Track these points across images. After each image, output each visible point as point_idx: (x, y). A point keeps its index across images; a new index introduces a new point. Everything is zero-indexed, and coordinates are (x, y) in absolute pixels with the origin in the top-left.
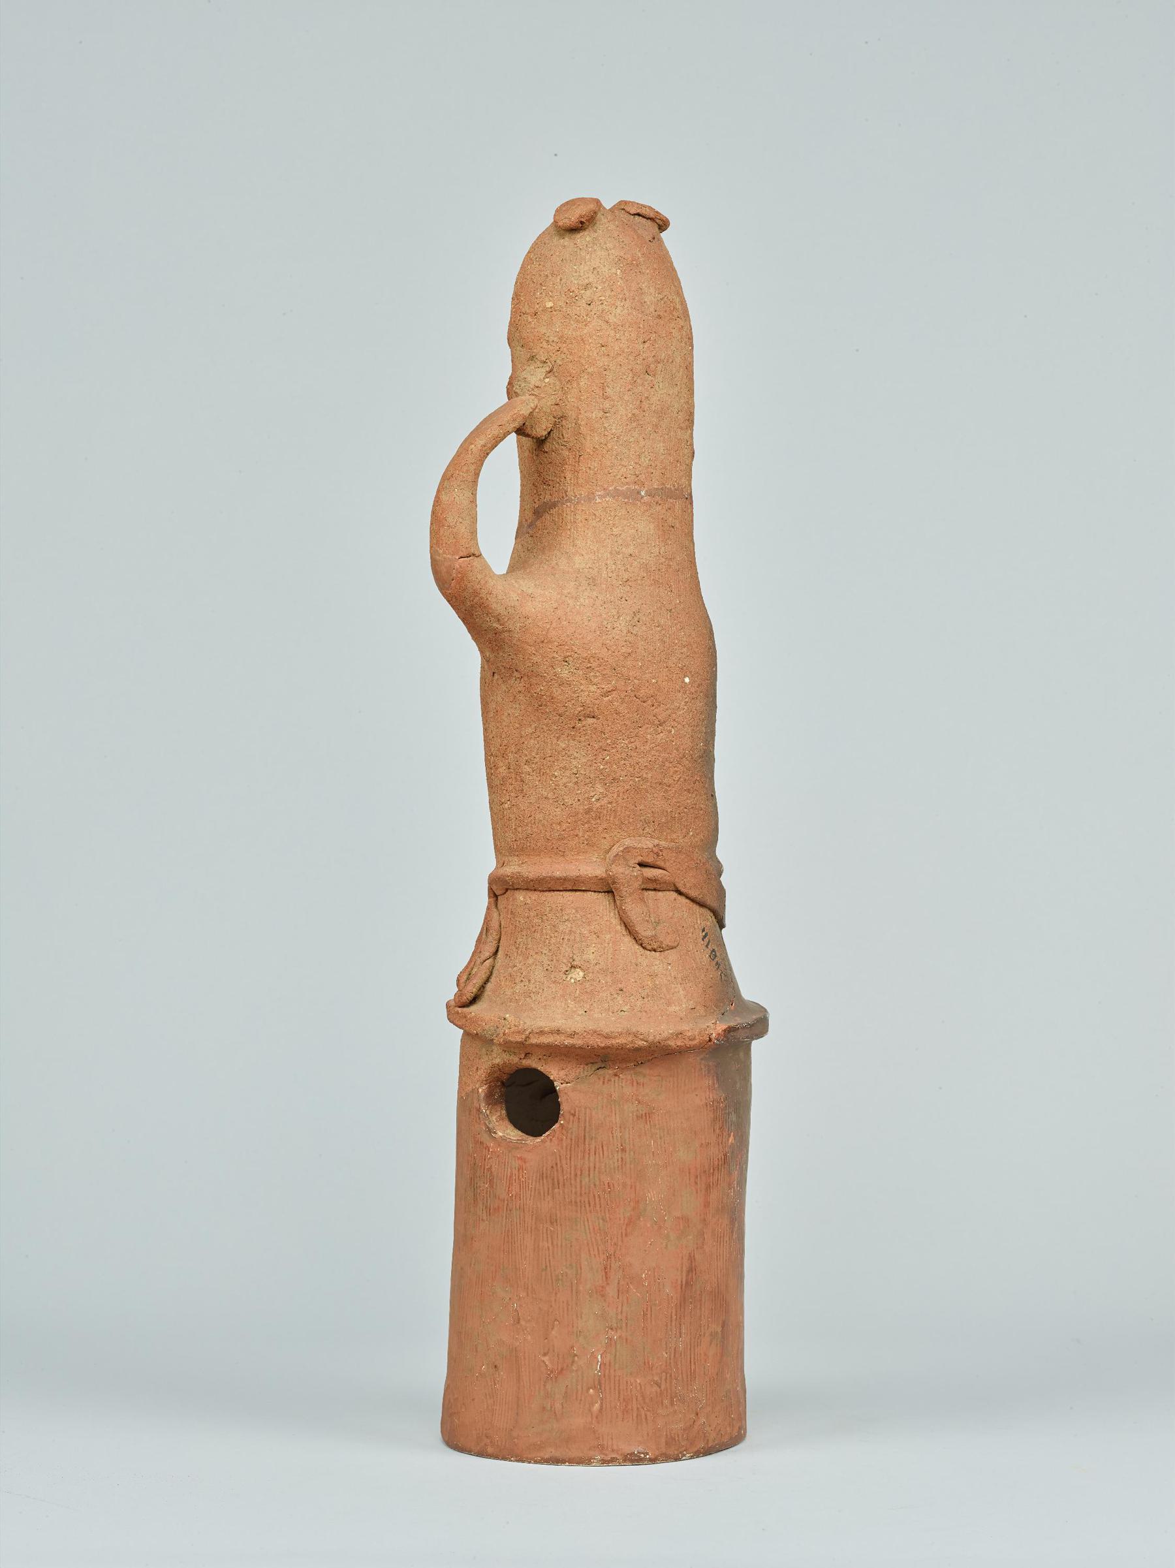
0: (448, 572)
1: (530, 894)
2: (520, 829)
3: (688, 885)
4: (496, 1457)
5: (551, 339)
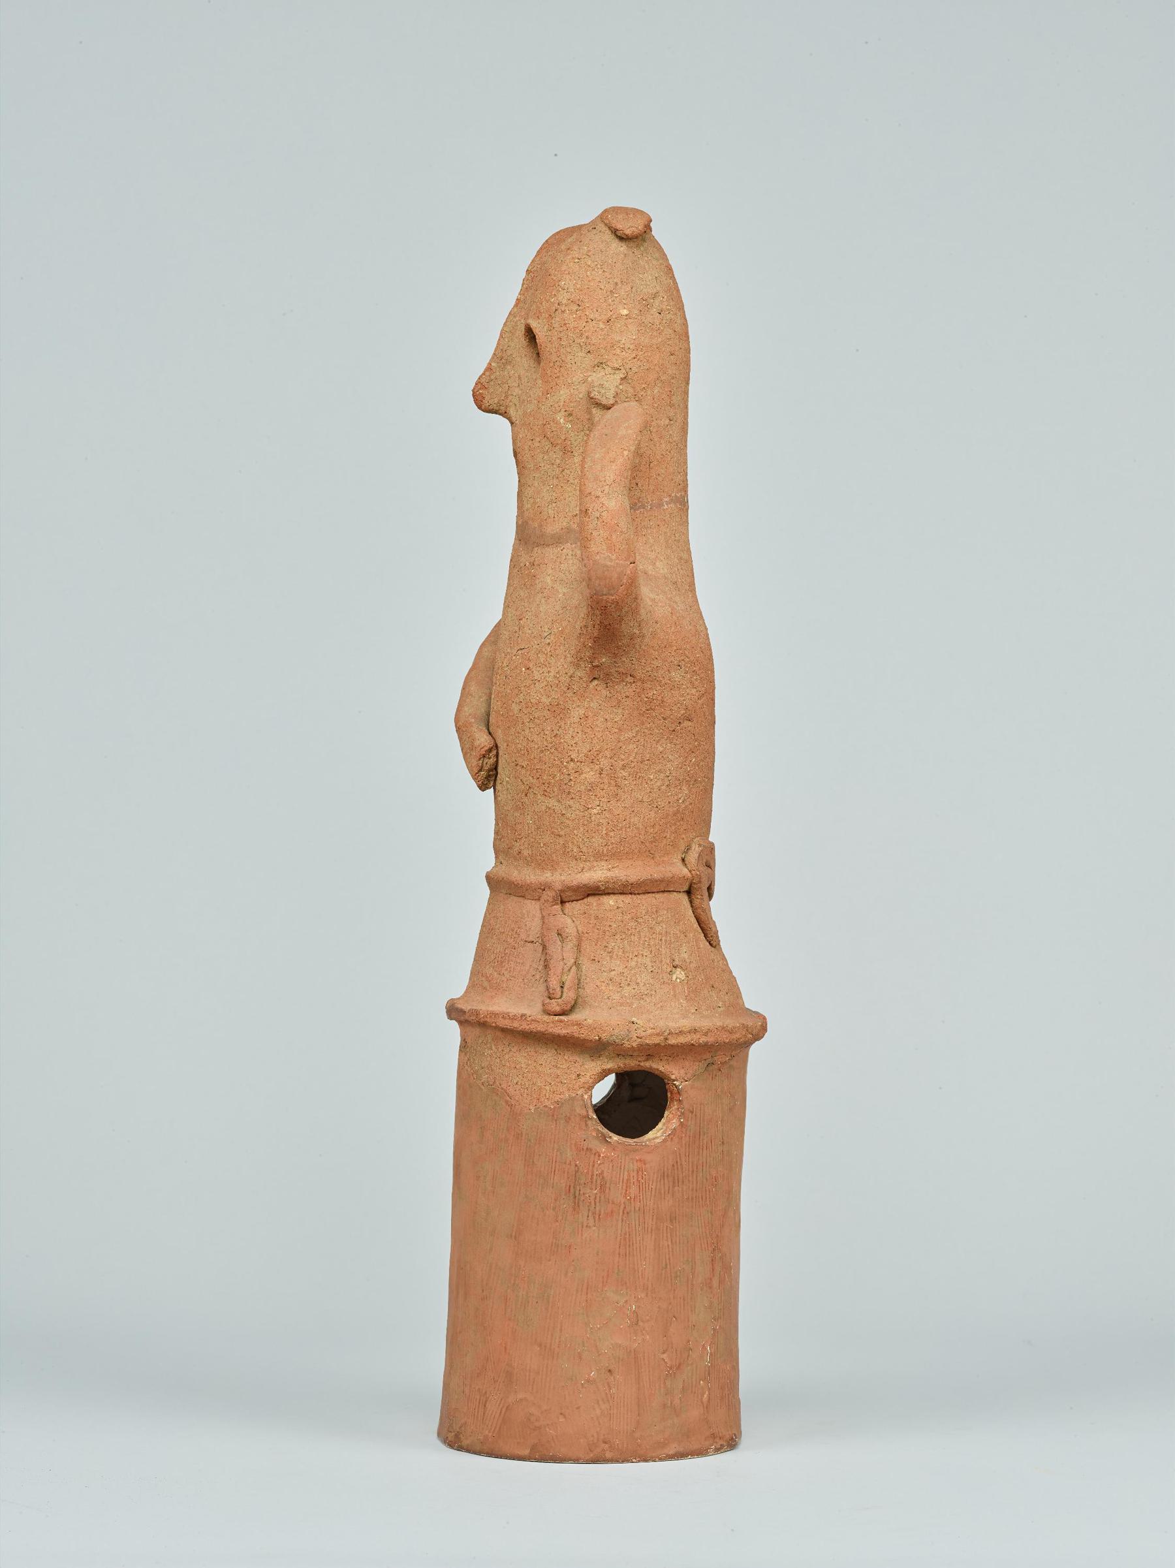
0: (619, 578)
1: (622, 897)
2: (612, 834)
4: (617, 1461)
5: (627, 346)
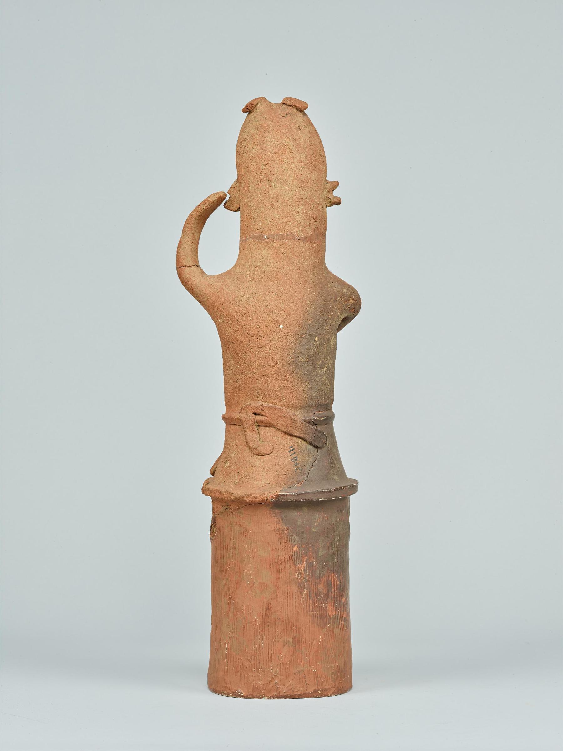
3: (279, 425)
